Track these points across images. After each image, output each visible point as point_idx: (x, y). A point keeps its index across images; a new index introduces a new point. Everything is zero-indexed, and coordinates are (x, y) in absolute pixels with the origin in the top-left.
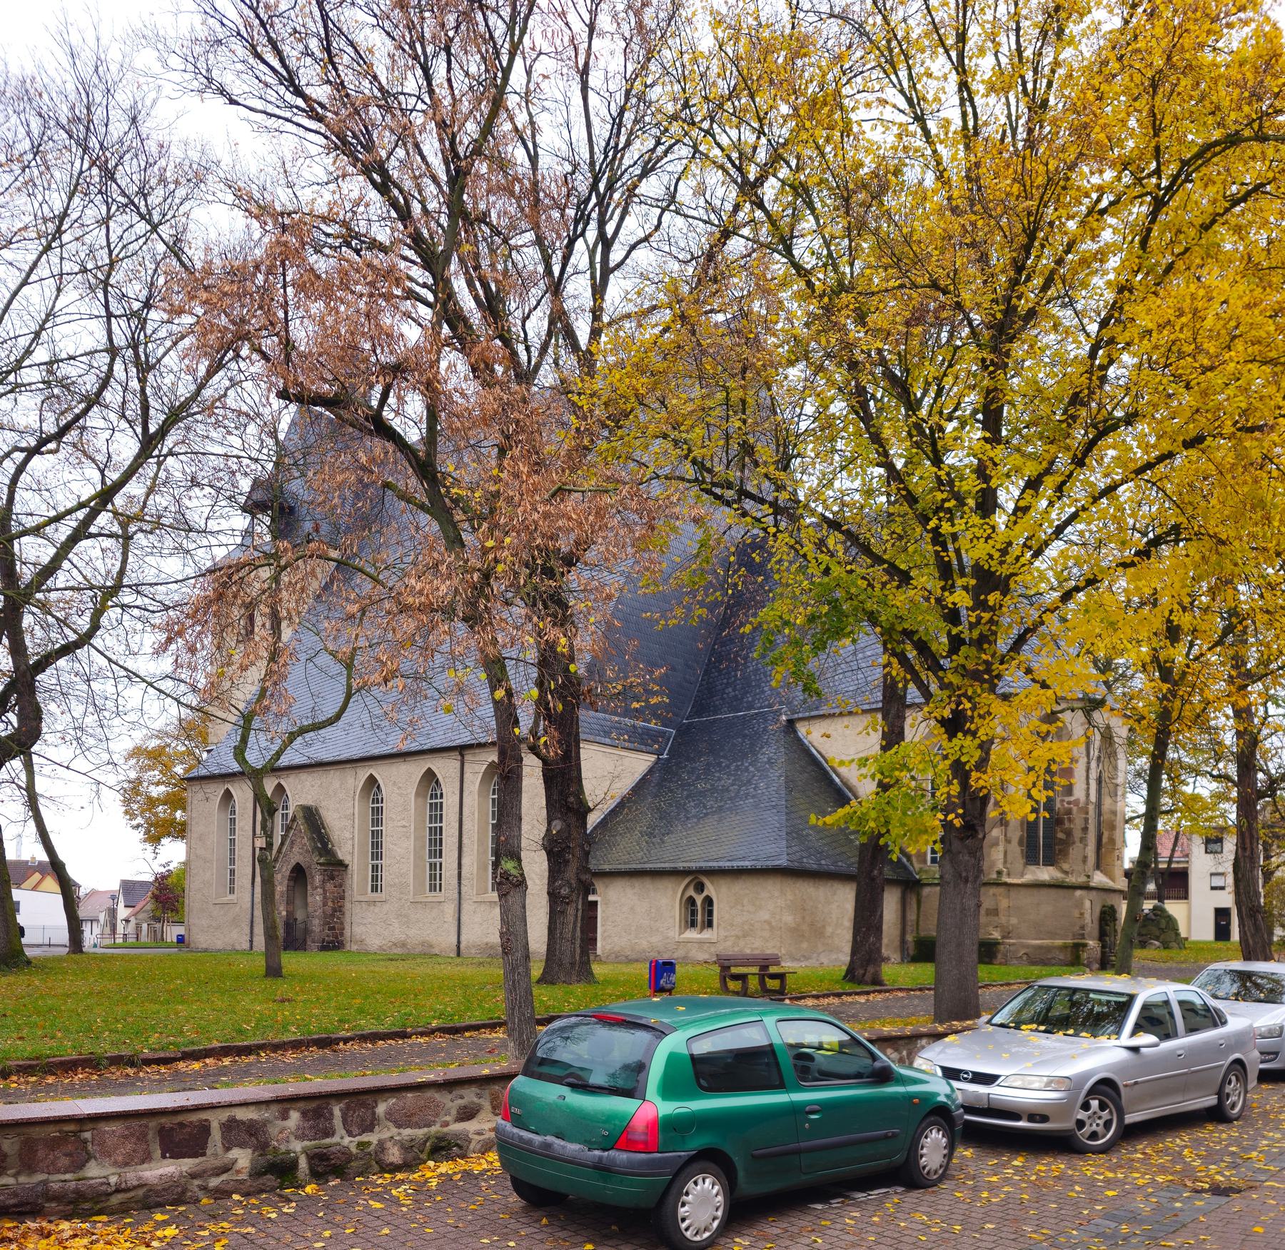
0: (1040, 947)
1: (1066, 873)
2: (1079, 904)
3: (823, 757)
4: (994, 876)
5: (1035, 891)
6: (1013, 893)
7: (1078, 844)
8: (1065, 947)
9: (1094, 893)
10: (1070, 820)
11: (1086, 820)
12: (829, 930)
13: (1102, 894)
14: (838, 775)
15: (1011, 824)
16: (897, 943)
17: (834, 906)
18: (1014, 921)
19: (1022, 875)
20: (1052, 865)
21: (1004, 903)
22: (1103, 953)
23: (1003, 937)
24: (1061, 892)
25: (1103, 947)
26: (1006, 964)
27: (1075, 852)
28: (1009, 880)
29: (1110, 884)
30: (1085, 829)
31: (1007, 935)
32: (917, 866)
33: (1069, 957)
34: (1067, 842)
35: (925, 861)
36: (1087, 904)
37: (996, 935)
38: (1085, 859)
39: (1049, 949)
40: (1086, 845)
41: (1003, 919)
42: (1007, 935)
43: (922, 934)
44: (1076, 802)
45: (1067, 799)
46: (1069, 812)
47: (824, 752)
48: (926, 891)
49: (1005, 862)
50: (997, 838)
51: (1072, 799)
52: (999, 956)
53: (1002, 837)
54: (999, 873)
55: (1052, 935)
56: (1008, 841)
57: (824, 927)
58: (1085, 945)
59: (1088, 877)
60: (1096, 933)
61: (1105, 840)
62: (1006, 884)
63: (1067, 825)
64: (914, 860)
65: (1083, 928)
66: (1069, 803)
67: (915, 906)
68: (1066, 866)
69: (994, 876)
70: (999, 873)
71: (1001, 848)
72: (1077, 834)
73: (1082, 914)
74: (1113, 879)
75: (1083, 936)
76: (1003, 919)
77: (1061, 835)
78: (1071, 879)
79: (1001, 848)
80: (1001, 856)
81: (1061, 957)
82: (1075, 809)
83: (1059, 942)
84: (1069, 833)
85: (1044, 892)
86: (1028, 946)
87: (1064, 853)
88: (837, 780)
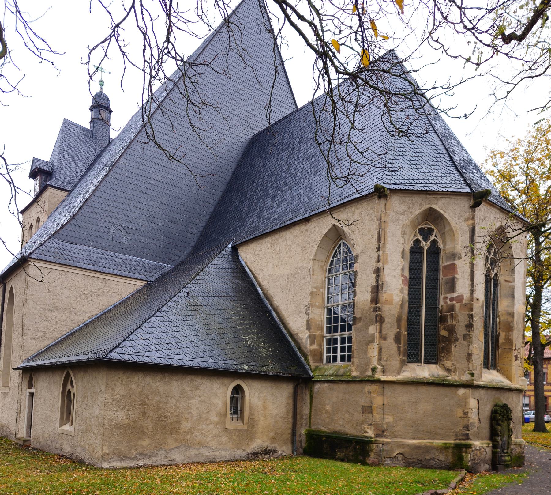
0: (417, 447)
1: (449, 371)
2: (464, 403)
3: (253, 274)
4: (370, 373)
5: (413, 389)
6: (388, 390)
7: (461, 341)
8: (445, 448)
9: (482, 392)
10: (452, 317)
11: (471, 317)
12: (186, 426)
13: (493, 393)
14: (261, 288)
15: (387, 320)
16: (288, 435)
17: (196, 401)
18: (389, 419)
19: (399, 373)
20: (435, 363)
21: (378, 401)
22: (494, 454)
23: (377, 436)
24: (442, 391)
25: (494, 447)
26: (377, 465)
27: (458, 350)
28: (383, 378)
29: (506, 382)
30: (470, 326)
31: (381, 433)
32: (313, 364)
33: (450, 459)
34: (451, 339)
35: (321, 360)
36: (473, 403)
37: (371, 433)
38: (469, 357)
39: (427, 449)
40: (470, 342)
41: (377, 417)
42: (381, 433)
43: (314, 427)
44: (460, 299)
45: (450, 296)
46: (452, 309)
47: (253, 270)
48: (317, 387)
49: (380, 359)
50: (373, 335)
51: (455, 295)
52: (372, 455)
53: (377, 334)
54: (374, 370)
55: (432, 435)
56: (383, 338)
57: (178, 422)
58: (469, 446)
59: (472, 375)
60: (486, 431)
61: (501, 340)
62: (379, 381)
63: (449, 322)
64: (310, 358)
65: (467, 427)
66: (452, 299)
67: (308, 400)
68: (448, 364)
69: (370, 373)
70: (374, 370)
71: (376, 345)
72: (461, 331)
73: (466, 414)
74: (510, 378)
75: (467, 437)
76: (377, 417)
77: (444, 333)
78: (454, 377)
79: (376, 345)
80: (376, 353)
81: (442, 458)
82: (458, 305)
83: (439, 442)
84: (451, 330)
85: (423, 390)
86: (403, 446)
87: (447, 351)
88: (260, 291)
